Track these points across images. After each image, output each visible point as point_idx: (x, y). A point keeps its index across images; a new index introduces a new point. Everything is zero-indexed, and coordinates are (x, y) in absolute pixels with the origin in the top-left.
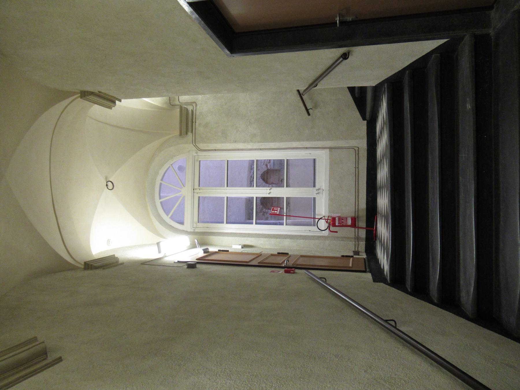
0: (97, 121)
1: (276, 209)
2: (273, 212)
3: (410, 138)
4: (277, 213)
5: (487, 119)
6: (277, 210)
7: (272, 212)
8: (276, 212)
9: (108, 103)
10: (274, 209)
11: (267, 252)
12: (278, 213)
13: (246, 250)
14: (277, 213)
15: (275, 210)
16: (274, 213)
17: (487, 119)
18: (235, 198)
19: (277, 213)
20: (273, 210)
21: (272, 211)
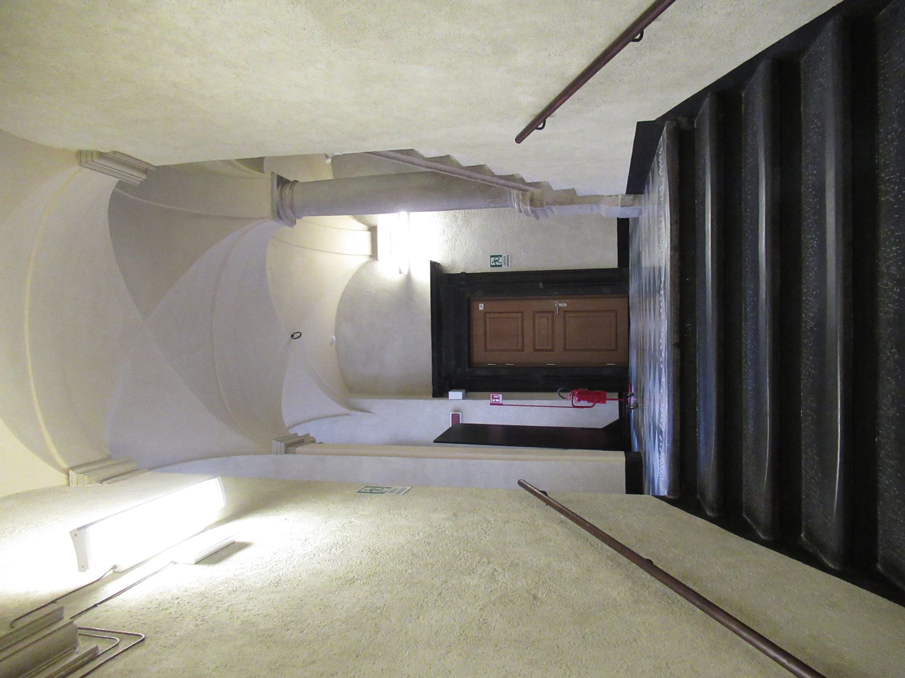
2: (494, 400)
6: (498, 398)
8: (497, 400)
10: (495, 396)
12: (501, 402)
15: (495, 398)
20: (493, 398)
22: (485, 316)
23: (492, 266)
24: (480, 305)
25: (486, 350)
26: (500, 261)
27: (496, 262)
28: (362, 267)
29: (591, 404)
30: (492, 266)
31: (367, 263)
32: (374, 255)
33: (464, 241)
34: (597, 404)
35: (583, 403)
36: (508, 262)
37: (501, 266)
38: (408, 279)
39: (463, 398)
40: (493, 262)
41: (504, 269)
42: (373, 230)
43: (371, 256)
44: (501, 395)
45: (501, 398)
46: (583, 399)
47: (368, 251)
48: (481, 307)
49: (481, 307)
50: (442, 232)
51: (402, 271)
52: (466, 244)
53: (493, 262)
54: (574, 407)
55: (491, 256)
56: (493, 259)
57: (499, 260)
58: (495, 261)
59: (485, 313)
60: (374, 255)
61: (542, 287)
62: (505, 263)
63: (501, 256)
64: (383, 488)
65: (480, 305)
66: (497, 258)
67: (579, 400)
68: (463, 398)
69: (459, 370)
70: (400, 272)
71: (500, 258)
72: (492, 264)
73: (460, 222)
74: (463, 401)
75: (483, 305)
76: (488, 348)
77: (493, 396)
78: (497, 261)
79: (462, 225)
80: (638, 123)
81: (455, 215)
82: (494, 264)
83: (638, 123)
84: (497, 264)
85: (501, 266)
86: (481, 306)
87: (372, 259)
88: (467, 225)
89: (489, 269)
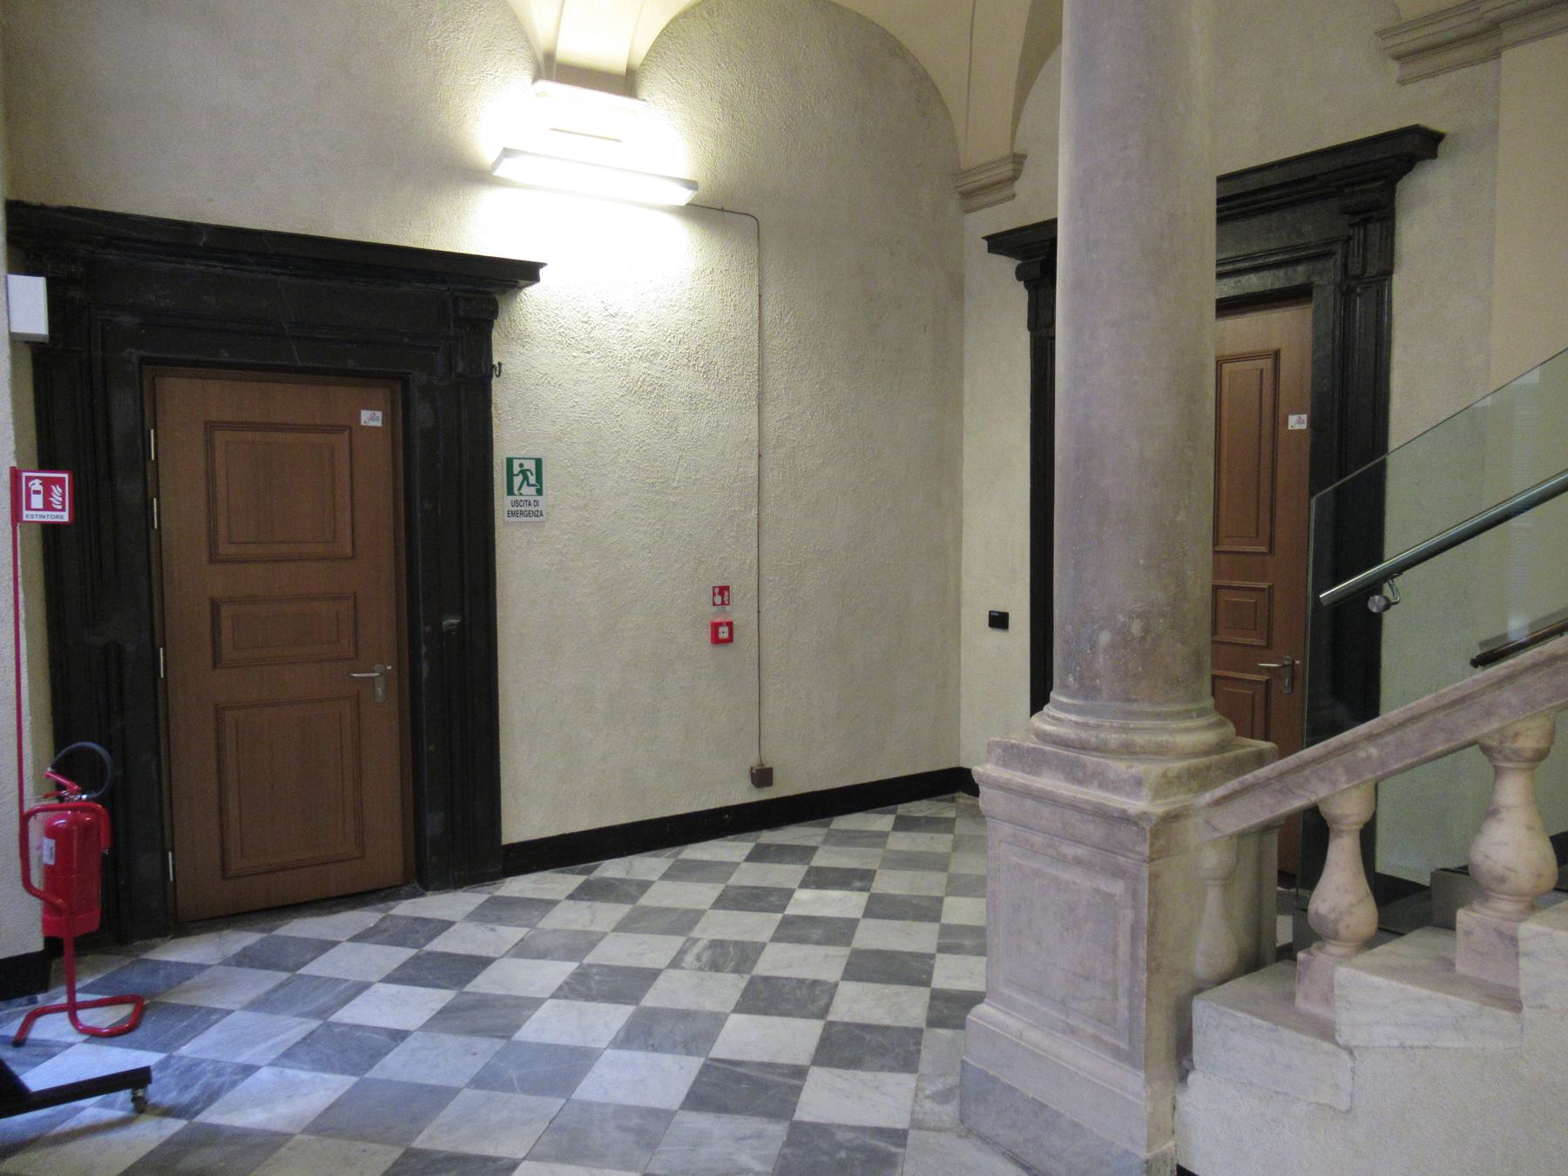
0: (1376, 800)
1: (56, 498)
2: (37, 485)
3: (406, 624)
4: (29, 508)
5: (1081, 497)
6: (48, 506)
7: (29, 479)
8: (37, 501)
9: (1493, 513)
10: (57, 490)
11: (5, 361)
12: (27, 515)
13: (1063, 860)
14: (29, 508)
15: (47, 494)
16: (28, 489)
17: (1081, 497)
18: (1054, 298)
19: (25, 513)
20: (47, 484)
21: (37, 482)
22: (338, 429)
23: (510, 461)
24: (379, 414)
25: (211, 427)
26: (525, 490)
27: (520, 478)
28: (515, 18)
29: (37, 880)
30: (510, 461)
31: (527, 40)
32: (552, 68)
33: (585, 377)
34: (35, 907)
35: (44, 851)
36: (522, 513)
37: (510, 492)
38: (474, 175)
39: (17, 341)
40: (521, 465)
41: (502, 503)
42: (625, 83)
43: (550, 57)
44: (65, 517)
45: (50, 517)
46: (62, 852)
47: (573, 49)
48: (371, 418)
49: (371, 418)
50: (612, 311)
51: (507, 162)
52: (576, 382)
53: (521, 465)
54: (25, 818)
55: (539, 462)
56: (530, 465)
57: (529, 485)
58: (524, 472)
59: (350, 427)
60: (552, 68)
61: (445, 623)
62: (516, 503)
63: (539, 492)
64: (164, 646)
65: (379, 414)
66: (532, 480)
67: (51, 832)
68: (17, 341)
69: (128, 320)
70: (507, 153)
71: (533, 490)
72: (516, 464)
73: (637, 368)
74: (7, 333)
75: (379, 424)
76: (220, 437)
77: (60, 482)
78: (526, 478)
79: (632, 375)
80: (771, 784)
81: (656, 354)
82: (516, 469)
83: (771, 784)
84: (517, 480)
85: (510, 492)
86: (372, 419)
87: (541, 59)
88: (629, 391)
89: (501, 452)
